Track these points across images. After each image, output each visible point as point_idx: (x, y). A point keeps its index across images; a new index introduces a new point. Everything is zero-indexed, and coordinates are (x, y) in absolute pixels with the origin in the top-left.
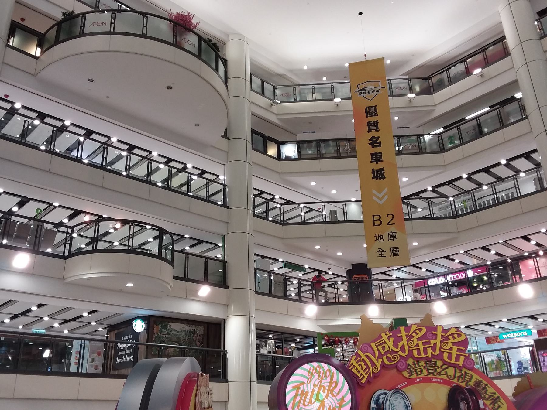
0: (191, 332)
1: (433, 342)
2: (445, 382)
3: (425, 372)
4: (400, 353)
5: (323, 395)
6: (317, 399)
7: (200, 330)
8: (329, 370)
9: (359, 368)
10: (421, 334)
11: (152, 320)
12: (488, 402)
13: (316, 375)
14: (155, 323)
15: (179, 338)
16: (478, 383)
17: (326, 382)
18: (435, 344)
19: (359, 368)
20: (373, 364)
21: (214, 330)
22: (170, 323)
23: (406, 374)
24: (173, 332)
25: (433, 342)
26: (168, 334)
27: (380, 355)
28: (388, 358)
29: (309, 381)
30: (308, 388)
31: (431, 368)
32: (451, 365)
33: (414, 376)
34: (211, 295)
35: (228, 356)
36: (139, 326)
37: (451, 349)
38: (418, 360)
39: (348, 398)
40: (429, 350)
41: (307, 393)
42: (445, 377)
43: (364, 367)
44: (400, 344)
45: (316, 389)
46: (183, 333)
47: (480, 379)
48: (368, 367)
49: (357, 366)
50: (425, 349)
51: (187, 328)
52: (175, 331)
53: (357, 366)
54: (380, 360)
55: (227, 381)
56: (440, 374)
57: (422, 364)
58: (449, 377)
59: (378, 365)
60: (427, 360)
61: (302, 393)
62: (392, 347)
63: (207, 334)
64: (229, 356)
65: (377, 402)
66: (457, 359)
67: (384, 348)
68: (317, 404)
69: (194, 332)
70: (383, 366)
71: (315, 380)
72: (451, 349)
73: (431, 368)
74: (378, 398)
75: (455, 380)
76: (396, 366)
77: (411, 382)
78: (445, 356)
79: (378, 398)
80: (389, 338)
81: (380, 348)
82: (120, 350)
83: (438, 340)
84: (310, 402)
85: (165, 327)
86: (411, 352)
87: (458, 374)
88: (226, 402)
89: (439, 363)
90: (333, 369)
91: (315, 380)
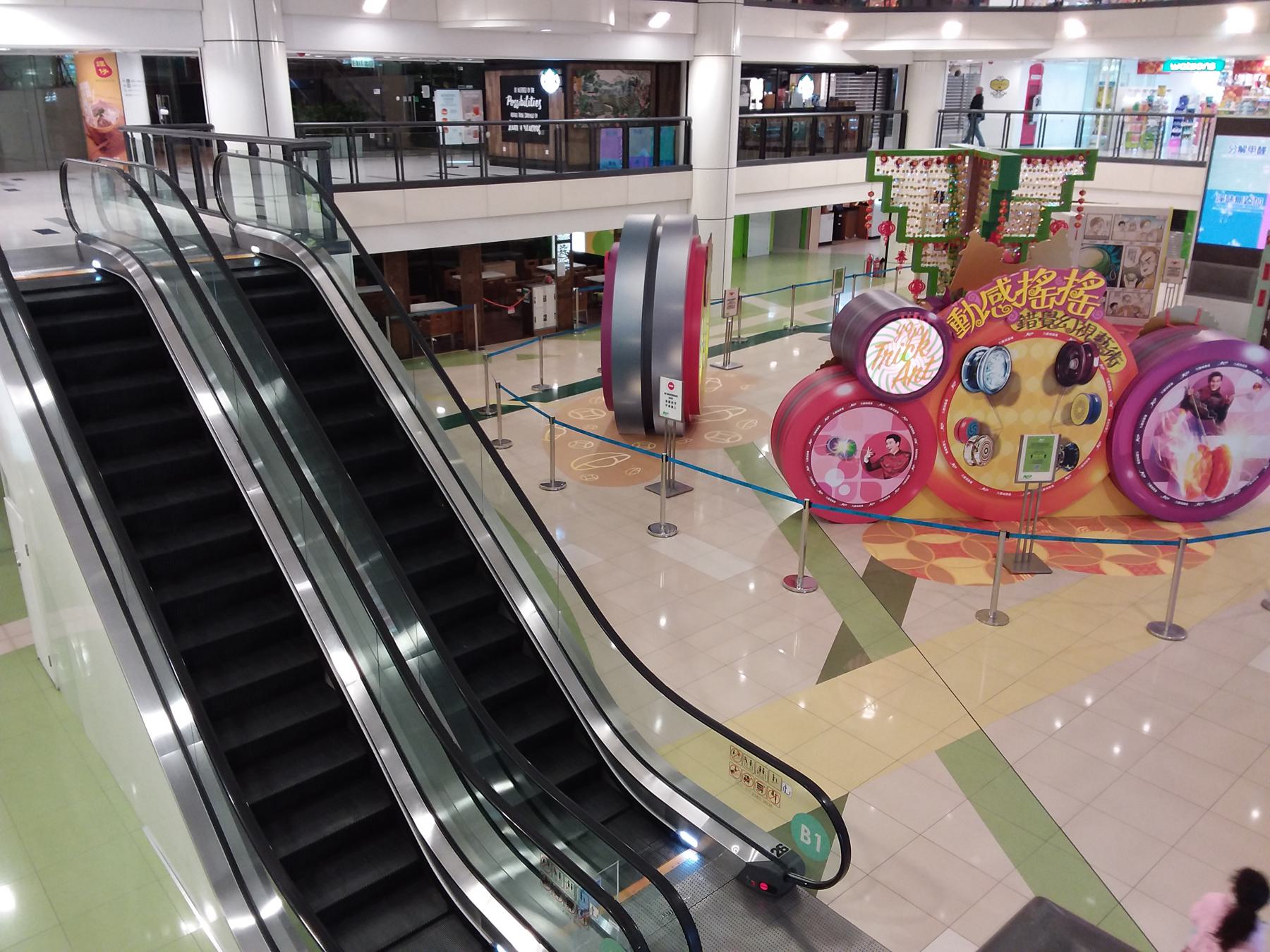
0: (631, 83)
1: (1060, 290)
2: (1061, 336)
3: (1039, 324)
4: (1015, 304)
5: (910, 354)
6: (903, 359)
7: (646, 78)
8: (922, 328)
9: (959, 322)
10: (1048, 280)
11: (570, 67)
12: (1104, 358)
13: (905, 334)
14: (575, 74)
15: (612, 96)
16: (1100, 338)
17: (916, 341)
18: (1062, 293)
19: (959, 322)
20: (977, 317)
21: (666, 81)
22: (598, 71)
23: (1015, 327)
24: (604, 87)
25: (1060, 290)
26: (596, 90)
27: (989, 307)
28: (999, 311)
29: (896, 340)
30: (894, 347)
31: (1048, 320)
32: (1073, 316)
33: (1025, 329)
34: (670, 24)
35: (693, 127)
36: (550, 82)
37: (1081, 298)
38: (1034, 312)
39: (941, 352)
40: (1053, 300)
41: (891, 353)
42: (1062, 330)
43: (966, 320)
44: (1018, 293)
45: (903, 349)
46: (619, 87)
47: (1104, 331)
48: (970, 321)
49: (957, 319)
50: (1048, 300)
51: (625, 76)
52: (607, 84)
53: (957, 319)
54: (988, 313)
55: (690, 168)
56: (1057, 326)
57: (1039, 315)
58: (1068, 330)
59: (984, 318)
60: (1046, 312)
61: (886, 353)
62: (1007, 297)
63: (656, 84)
64: (694, 127)
65: (971, 361)
66: (1084, 311)
67: (995, 298)
68: (903, 363)
69: (635, 84)
70: (990, 318)
71: (904, 338)
72: (1081, 298)
73: (1048, 320)
74: (975, 356)
75: (1073, 334)
76: (1006, 319)
77: (1019, 336)
78: (1071, 306)
79: (975, 356)
80: (1005, 286)
81: (991, 298)
82: (512, 109)
83: (1067, 289)
84: (894, 362)
85: (590, 79)
86: (1029, 302)
87: (1079, 327)
88: (688, 201)
89: (1060, 314)
90: (927, 326)
91: (904, 338)
